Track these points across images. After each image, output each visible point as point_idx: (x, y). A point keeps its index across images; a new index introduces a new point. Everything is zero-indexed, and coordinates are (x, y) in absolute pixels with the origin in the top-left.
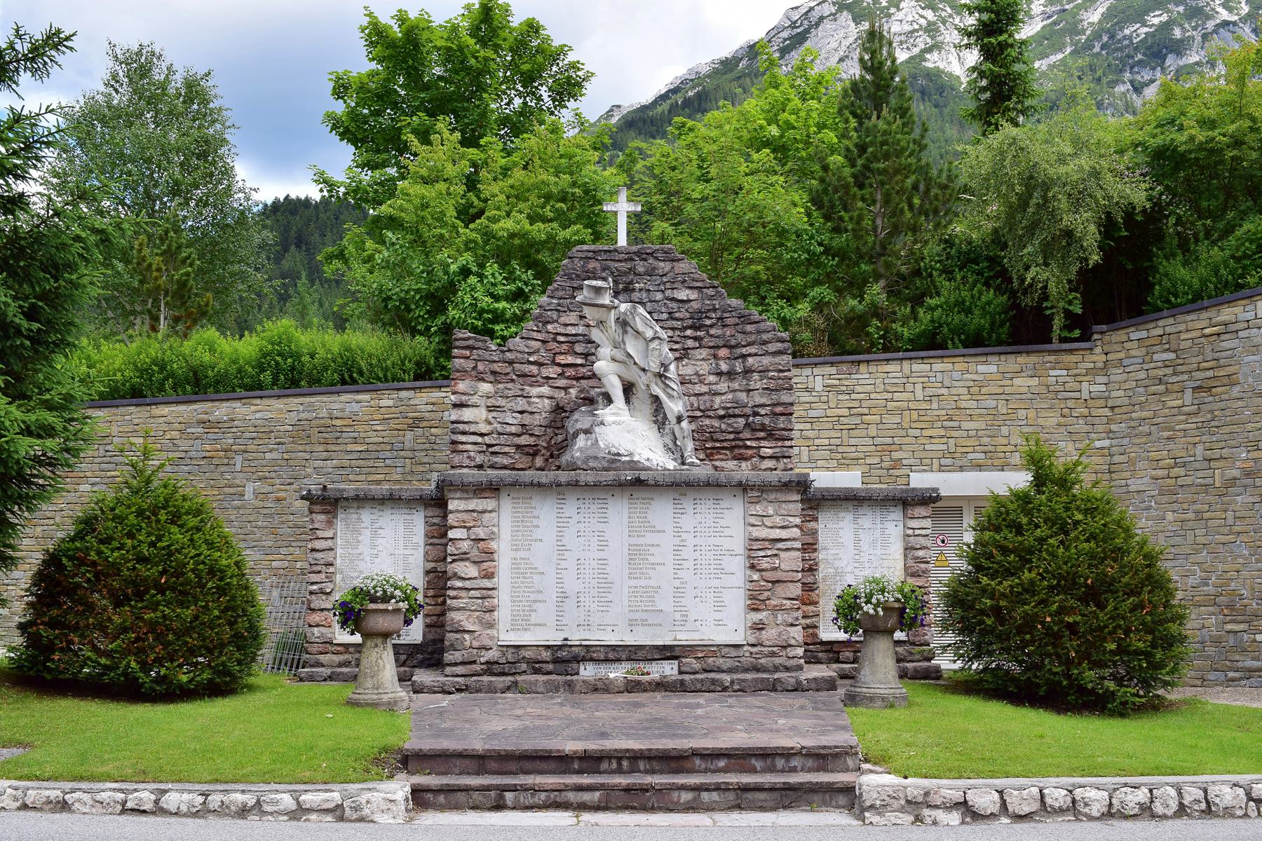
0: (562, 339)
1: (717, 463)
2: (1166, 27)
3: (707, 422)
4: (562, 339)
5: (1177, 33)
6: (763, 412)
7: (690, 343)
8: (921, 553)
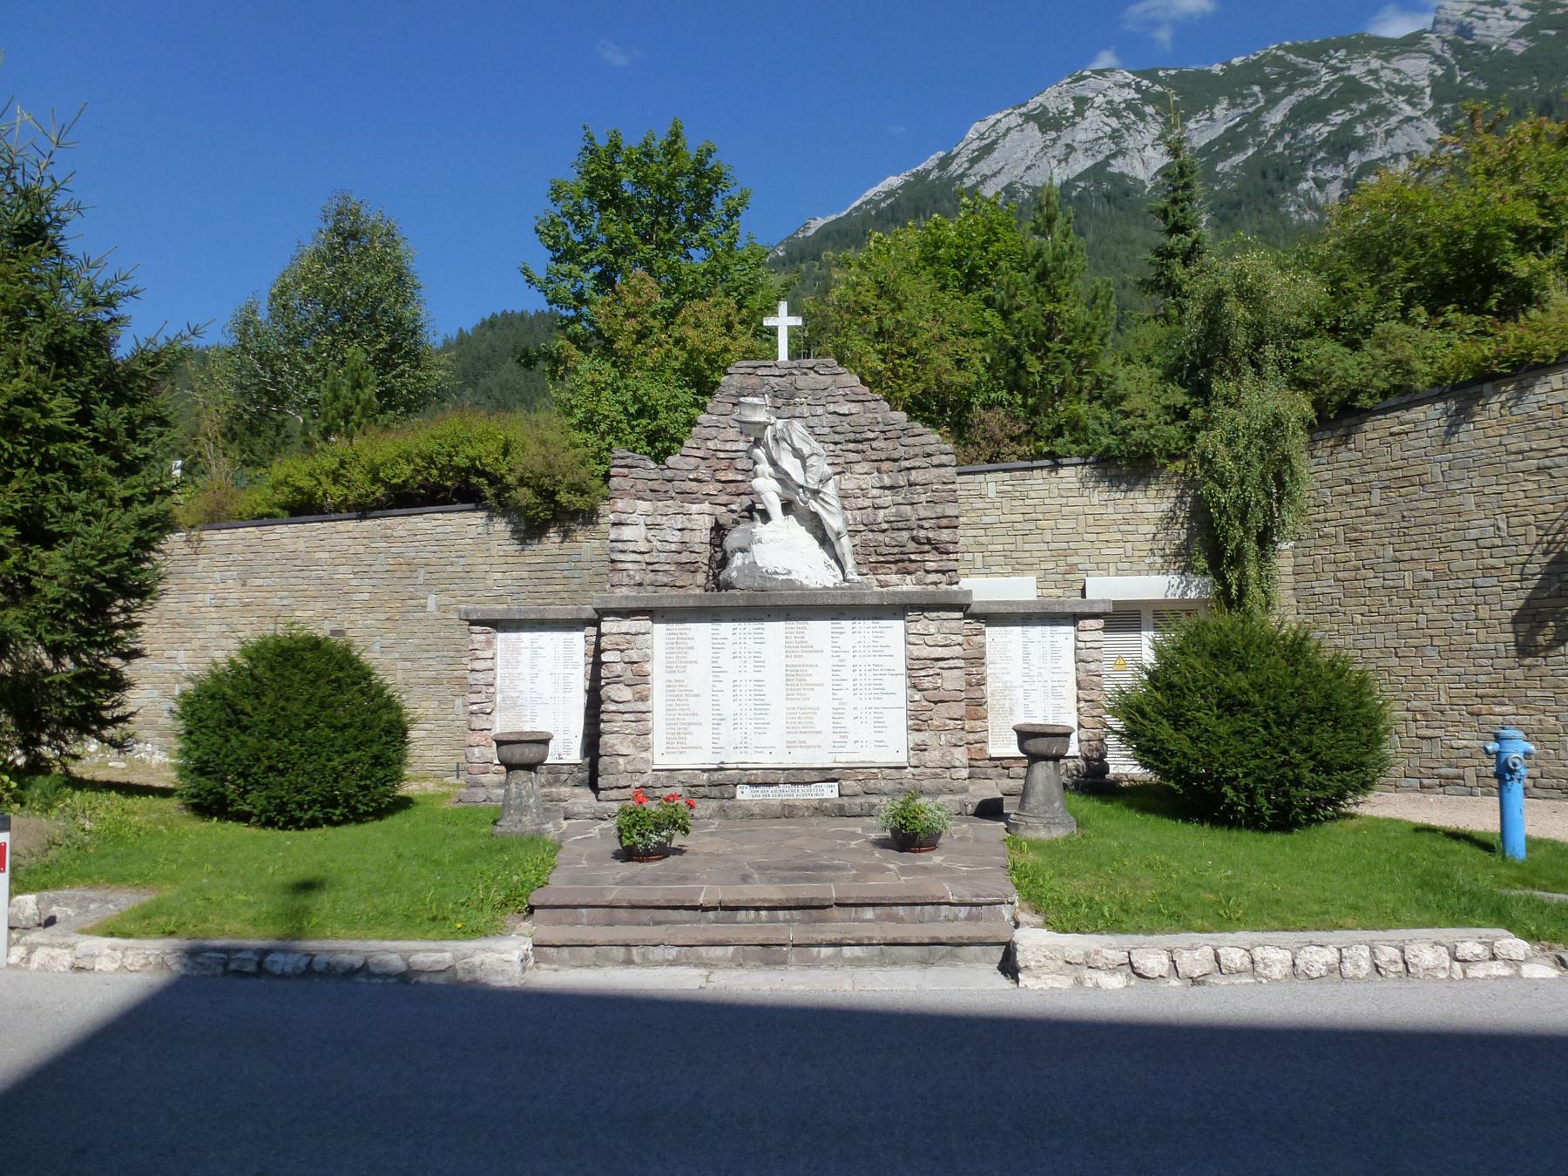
0: (722, 455)
1: (881, 577)
2: (1348, 126)
3: (871, 535)
4: (722, 455)
5: (1360, 130)
6: (926, 524)
7: (852, 457)
8: (1093, 666)
